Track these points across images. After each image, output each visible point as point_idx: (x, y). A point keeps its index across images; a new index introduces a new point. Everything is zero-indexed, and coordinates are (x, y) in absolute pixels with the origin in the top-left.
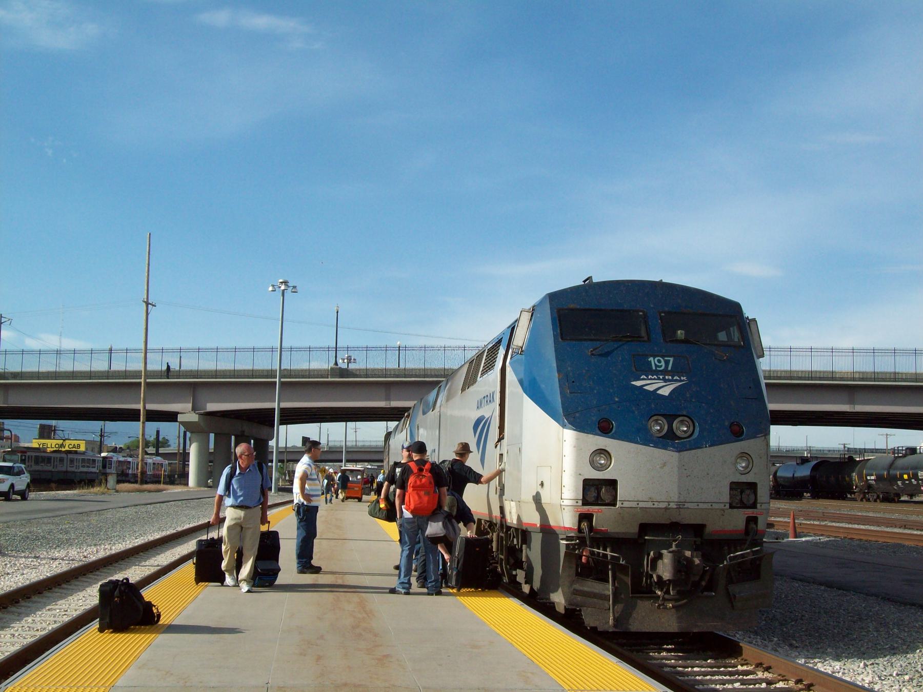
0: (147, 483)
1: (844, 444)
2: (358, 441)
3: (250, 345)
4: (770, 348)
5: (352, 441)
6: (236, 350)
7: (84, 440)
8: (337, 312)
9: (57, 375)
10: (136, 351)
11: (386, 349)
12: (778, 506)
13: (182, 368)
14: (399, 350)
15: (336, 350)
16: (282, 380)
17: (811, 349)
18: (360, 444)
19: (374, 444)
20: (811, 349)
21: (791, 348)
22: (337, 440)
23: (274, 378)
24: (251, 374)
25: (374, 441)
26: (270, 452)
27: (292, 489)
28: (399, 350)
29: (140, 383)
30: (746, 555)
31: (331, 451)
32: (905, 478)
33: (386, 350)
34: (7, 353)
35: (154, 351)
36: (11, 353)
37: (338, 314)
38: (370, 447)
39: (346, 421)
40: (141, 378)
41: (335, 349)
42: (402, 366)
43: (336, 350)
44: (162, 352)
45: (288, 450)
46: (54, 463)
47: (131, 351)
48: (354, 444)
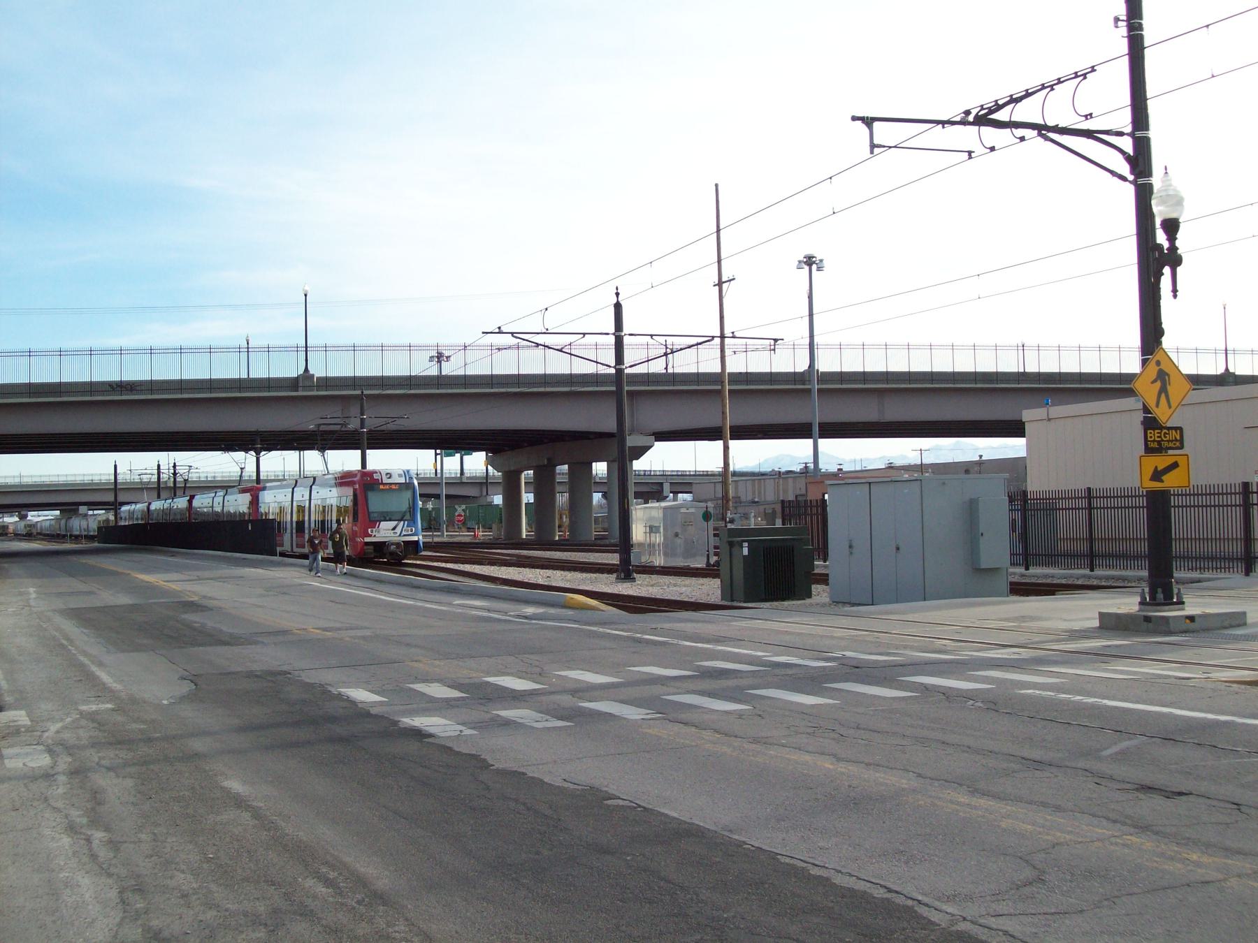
0: (1051, 558)
1: (806, 463)
4: (91, 351)
7: (807, 491)
9: (184, 386)
12: (77, 546)
14: (248, 352)
15: (306, 351)
16: (720, 387)
17: (297, 347)
19: (96, 479)
20: (30, 352)
21: (30, 352)
23: (820, 389)
24: (1058, 378)
25: (72, 475)
28: (248, 352)
29: (447, 531)
30: (1172, 626)
33: (181, 353)
34: (1195, 351)
35: (829, 347)
36: (877, 347)
38: (92, 484)
40: (819, 390)
41: (308, 349)
43: (306, 351)
44: (181, 353)
46: (812, 536)
47: (800, 347)
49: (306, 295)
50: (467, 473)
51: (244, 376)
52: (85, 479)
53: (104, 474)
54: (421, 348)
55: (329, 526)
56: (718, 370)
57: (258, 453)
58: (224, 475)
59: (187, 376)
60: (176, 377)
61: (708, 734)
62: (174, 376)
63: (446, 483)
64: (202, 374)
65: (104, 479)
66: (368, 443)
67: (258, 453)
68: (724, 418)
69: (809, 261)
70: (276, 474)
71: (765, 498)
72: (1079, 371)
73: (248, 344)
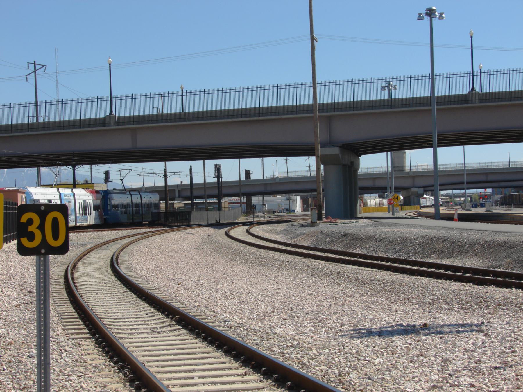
2: (290, 172)
3: (237, 85)
5: (284, 172)
6: (223, 91)
8: (472, 37)
10: (103, 99)
11: (98, 99)
13: (483, 92)
14: (182, 95)
15: (481, 75)
16: (312, 115)
18: (292, 175)
22: (489, 162)
25: (372, 168)
26: (359, 179)
27: (473, 207)
28: (182, 95)
31: (281, 183)
32: (43, 207)
35: (325, 84)
37: (473, 38)
38: (474, 170)
39: (239, 157)
42: (185, 111)
43: (481, 75)
45: (241, 184)
48: (286, 175)
49: (110, 64)
50: (441, 167)
51: (61, 119)
52: (374, 171)
53: (369, 168)
54: (379, 80)
55: (89, 212)
56: (311, 102)
57: (74, 167)
58: (452, 166)
59: (357, 99)
60: (369, 98)
61: (87, 343)
62: (292, 103)
63: (466, 174)
64: (348, 98)
65: (426, 168)
66: (438, 143)
67: (74, 167)
68: (316, 136)
69: (430, 13)
70: (498, 164)
71: (222, 192)
72: (221, 109)
73: (182, 90)
